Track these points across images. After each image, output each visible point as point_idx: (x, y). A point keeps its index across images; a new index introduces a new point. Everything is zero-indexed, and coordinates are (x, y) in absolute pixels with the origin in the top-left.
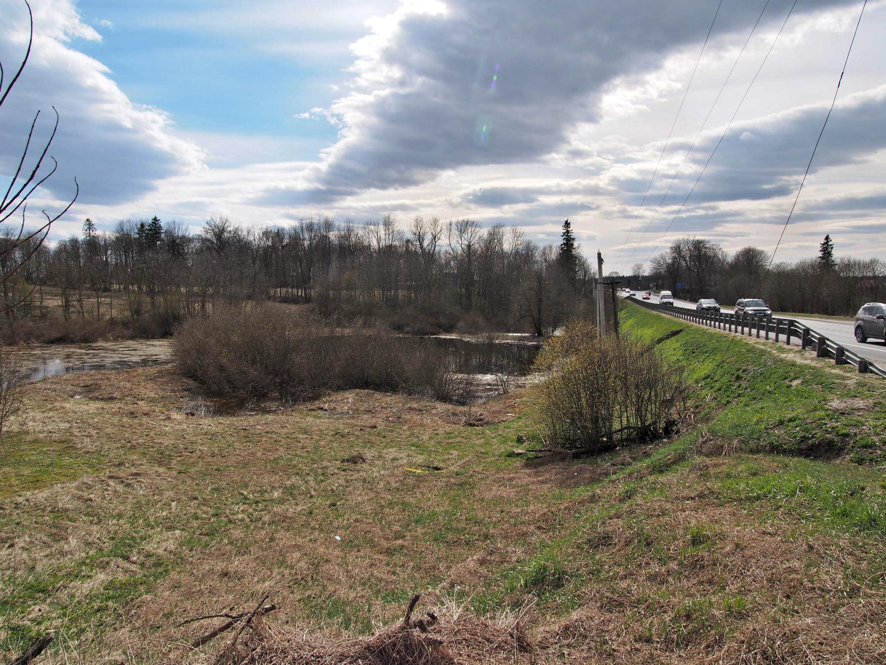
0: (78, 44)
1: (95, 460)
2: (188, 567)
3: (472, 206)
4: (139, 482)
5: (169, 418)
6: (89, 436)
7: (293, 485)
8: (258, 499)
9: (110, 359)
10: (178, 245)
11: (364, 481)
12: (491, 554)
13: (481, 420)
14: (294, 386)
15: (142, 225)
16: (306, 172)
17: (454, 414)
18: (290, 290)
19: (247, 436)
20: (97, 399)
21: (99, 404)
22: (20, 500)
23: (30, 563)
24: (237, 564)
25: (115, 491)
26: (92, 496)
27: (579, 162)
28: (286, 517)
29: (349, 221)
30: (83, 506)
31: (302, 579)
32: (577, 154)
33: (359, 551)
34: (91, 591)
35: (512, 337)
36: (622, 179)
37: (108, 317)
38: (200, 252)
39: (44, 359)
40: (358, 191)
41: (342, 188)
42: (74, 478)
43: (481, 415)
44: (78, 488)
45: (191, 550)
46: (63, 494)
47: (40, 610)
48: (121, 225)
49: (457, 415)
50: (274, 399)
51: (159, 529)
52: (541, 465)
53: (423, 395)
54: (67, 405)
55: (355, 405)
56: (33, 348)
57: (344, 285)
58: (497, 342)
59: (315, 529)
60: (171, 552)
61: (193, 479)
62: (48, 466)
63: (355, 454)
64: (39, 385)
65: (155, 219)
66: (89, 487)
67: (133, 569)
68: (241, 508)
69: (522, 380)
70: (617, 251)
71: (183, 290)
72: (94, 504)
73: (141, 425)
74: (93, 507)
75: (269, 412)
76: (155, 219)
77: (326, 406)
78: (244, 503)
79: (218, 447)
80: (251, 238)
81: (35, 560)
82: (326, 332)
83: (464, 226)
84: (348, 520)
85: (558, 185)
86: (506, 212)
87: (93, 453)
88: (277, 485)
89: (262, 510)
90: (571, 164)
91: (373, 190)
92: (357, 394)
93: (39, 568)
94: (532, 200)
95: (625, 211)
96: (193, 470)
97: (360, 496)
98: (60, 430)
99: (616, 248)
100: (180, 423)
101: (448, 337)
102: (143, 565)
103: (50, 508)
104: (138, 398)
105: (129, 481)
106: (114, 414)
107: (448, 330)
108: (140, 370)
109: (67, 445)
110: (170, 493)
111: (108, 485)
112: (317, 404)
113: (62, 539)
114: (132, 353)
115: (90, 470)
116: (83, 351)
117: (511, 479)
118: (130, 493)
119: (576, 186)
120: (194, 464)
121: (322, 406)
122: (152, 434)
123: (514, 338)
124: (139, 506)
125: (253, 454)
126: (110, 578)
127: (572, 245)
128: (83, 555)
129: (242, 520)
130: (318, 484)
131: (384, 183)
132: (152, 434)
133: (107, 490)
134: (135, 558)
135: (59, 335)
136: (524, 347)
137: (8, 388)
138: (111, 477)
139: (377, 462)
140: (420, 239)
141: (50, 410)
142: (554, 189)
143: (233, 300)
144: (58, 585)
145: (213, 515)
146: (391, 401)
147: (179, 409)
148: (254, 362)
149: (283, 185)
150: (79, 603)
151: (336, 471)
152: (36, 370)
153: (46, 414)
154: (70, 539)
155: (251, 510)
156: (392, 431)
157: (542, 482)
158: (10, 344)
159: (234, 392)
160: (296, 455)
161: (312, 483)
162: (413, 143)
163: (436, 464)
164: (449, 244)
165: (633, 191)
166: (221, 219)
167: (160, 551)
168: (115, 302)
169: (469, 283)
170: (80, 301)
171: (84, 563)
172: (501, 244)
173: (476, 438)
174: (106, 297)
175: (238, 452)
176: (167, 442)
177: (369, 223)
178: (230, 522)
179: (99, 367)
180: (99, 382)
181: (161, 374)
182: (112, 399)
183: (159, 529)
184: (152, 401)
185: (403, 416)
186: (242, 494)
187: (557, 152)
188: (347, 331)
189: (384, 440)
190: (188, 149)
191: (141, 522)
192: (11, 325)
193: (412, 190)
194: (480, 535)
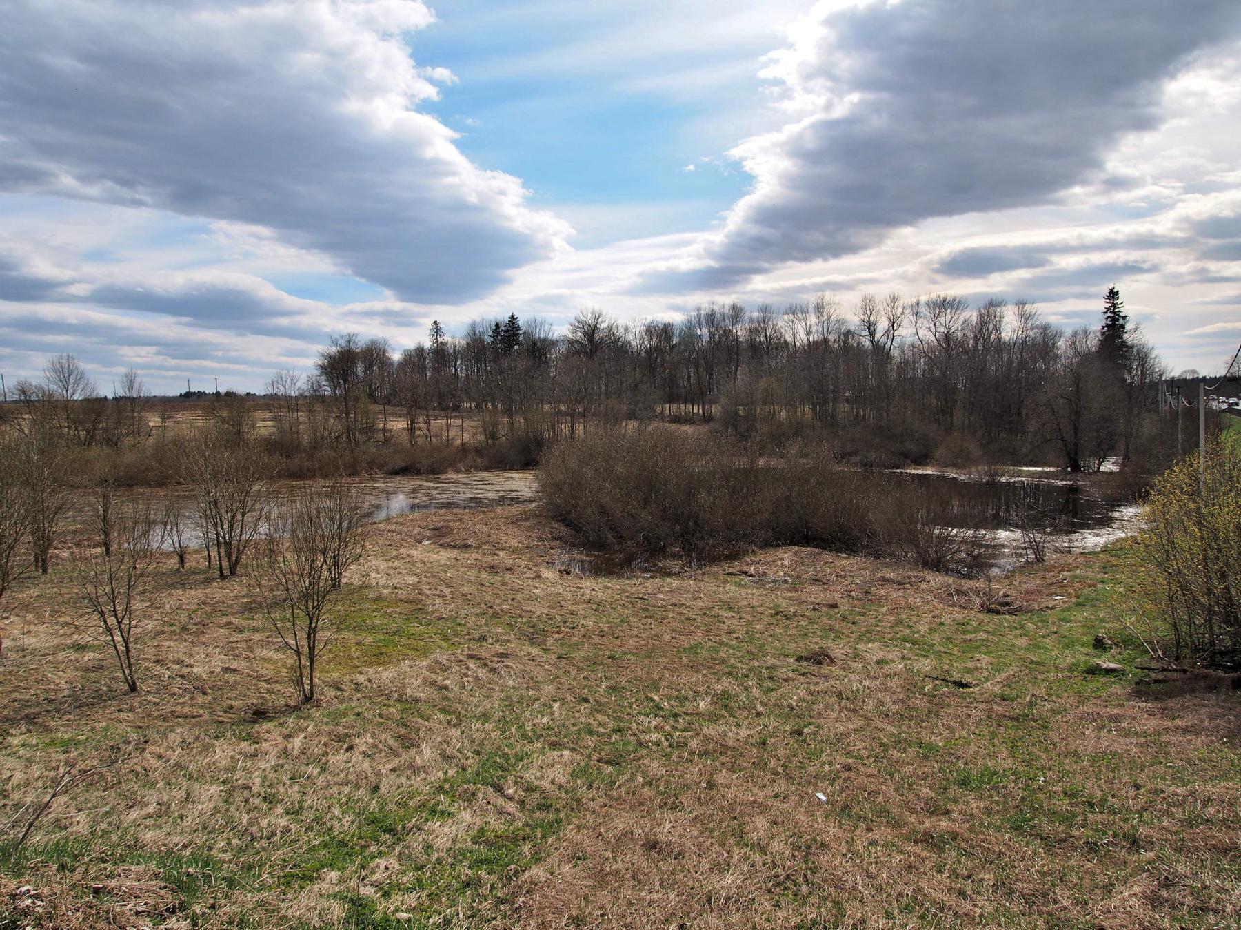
0: (425, 107)
1: (450, 632)
2: (590, 819)
3: (939, 277)
4: (507, 666)
5: (539, 577)
6: (442, 596)
7: (725, 692)
8: (676, 710)
9: (464, 495)
10: (539, 349)
11: (840, 695)
12: (1167, 886)
13: (1007, 604)
14: (702, 538)
15: (497, 326)
16: (698, 247)
17: (958, 592)
18: (682, 406)
19: (646, 608)
20: (449, 546)
21: (452, 553)
22: (361, 679)
23: (373, 779)
24: (667, 828)
25: (477, 678)
26: (448, 682)
27: (1121, 196)
28: (727, 747)
29: (764, 309)
30: (436, 696)
31: (788, 877)
32: (1117, 183)
33: (869, 830)
34: (455, 841)
35: (1028, 473)
36: (1197, 218)
37: (459, 442)
38: (566, 358)
39: (388, 493)
40: (765, 265)
41: (746, 264)
42: (425, 653)
43: (1005, 595)
44: (430, 669)
45: (590, 787)
46: (409, 674)
47: (387, 868)
48: (473, 326)
49: (964, 593)
50: (675, 556)
51: (539, 745)
52: (1168, 695)
53: (899, 560)
54: (415, 553)
55: (794, 570)
56: (375, 480)
57: (759, 396)
58: (1004, 479)
59: (778, 774)
60: (561, 786)
61: (579, 669)
62: (394, 634)
63: (816, 648)
64: (382, 526)
65: (512, 317)
66: (444, 669)
67: (510, 810)
68: (654, 723)
69: (1063, 542)
70: (1190, 336)
71: (547, 407)
72: (451, 695)
73: (504, 584)
74: (449, 700)
75: (669, 574)
76: (512, 317)
77: (752, 570)
78: (657, 716)
79: (608, 622)
80: (630, 337)
81: (378, 774)
82: (742, 462)
83: (942, 305)
84: (830, 764)
85: (1079, 237)
86: (995, 284)
87: (446, 620)
88: (701, 689)
89: (685, 730)
90: (1102, 201)
91: (791, 263)
92: (796, 554)
93: (384, 789)
94: (1040, 264)
95: (1203, 271)
96: (577, 655)
97: (836, 723)
98: (406, 586)
99: (1197, 331)
100: (554, 585)
101: (920, 472)
102: (522, 803)
103: (396, 695)
104: (498, 547)
105: (495, 665)
106: (470, 567)
107: (920, 461)
108: (499, 510)
109: (415, 607)
110: (548, 688)
111: (468, 668)
112: (737, 566)
113: (413, 745)
114: (488, 487)
115: (443, 644)
116: (431, 484)
117: (1117, 719)
118: (497, 683)
119: (1113, 236)
120: (577, 646)
121: (745, 569)
122: (519, 597)
123: (1032, 475)
124: (508, 703)
125: (658, 637)
126: (479, 822)
127: (1123, 326)
128: (441, 774)
129: (658, 744)
130: (766, 693)
131: (807, 253)
132: (519, 597)
133: (466, 675)
134: (511, 791)
135: (403, 465)
136: (1051, 489)
137: (349, 528)
138: (471, 657)
139: (854, 665)
140: (870, 326)
141: (396, 558)
142: (1073, 243)
143: (613, 418)
144: (410, 825)
145: (614, 731)
146: (851, 568)
147: (550, 564)
148: (646, 501)
149: (662, 266)
150: (439, 861)
151: (791, 674)
152: (378, 507)
153: (390, 564)
154: (423, 746)
155: (668, 728)
156: (864, 614)
157: (1186, 731)
158: (351, 475)
159: (619, 543)
160: (722, 643)
161: (755, 692)
162: (855, 190)
163: (956, 676)
164: (914, 333)
165: (1215, 236)
166: (593, 313)
167: (545, 783)
168: (467, 423)
169: (948, 394)
170: (427, 422)
171: (440, 789)
172: (998, 329)
173: (1016, 637)
174: (456, 417)
175: (636, 632)
176: (540, 610)
177: (792, 310)
178: (640, 744)
179: (448, 505)
180: (451, 524)
181: (525, 516)
182: (466, 547)
183: (539, 745)
184: (515, 551)
185: (873, 590)
186: (652, 700)
187: (1084, 183)
188: (774, 462)
189: (854, 628)
190: (550, 225)
191: (513, 729)
192: (352, 451)
193: (848, 261)
194: (1115, 836)
